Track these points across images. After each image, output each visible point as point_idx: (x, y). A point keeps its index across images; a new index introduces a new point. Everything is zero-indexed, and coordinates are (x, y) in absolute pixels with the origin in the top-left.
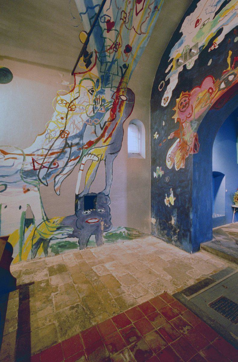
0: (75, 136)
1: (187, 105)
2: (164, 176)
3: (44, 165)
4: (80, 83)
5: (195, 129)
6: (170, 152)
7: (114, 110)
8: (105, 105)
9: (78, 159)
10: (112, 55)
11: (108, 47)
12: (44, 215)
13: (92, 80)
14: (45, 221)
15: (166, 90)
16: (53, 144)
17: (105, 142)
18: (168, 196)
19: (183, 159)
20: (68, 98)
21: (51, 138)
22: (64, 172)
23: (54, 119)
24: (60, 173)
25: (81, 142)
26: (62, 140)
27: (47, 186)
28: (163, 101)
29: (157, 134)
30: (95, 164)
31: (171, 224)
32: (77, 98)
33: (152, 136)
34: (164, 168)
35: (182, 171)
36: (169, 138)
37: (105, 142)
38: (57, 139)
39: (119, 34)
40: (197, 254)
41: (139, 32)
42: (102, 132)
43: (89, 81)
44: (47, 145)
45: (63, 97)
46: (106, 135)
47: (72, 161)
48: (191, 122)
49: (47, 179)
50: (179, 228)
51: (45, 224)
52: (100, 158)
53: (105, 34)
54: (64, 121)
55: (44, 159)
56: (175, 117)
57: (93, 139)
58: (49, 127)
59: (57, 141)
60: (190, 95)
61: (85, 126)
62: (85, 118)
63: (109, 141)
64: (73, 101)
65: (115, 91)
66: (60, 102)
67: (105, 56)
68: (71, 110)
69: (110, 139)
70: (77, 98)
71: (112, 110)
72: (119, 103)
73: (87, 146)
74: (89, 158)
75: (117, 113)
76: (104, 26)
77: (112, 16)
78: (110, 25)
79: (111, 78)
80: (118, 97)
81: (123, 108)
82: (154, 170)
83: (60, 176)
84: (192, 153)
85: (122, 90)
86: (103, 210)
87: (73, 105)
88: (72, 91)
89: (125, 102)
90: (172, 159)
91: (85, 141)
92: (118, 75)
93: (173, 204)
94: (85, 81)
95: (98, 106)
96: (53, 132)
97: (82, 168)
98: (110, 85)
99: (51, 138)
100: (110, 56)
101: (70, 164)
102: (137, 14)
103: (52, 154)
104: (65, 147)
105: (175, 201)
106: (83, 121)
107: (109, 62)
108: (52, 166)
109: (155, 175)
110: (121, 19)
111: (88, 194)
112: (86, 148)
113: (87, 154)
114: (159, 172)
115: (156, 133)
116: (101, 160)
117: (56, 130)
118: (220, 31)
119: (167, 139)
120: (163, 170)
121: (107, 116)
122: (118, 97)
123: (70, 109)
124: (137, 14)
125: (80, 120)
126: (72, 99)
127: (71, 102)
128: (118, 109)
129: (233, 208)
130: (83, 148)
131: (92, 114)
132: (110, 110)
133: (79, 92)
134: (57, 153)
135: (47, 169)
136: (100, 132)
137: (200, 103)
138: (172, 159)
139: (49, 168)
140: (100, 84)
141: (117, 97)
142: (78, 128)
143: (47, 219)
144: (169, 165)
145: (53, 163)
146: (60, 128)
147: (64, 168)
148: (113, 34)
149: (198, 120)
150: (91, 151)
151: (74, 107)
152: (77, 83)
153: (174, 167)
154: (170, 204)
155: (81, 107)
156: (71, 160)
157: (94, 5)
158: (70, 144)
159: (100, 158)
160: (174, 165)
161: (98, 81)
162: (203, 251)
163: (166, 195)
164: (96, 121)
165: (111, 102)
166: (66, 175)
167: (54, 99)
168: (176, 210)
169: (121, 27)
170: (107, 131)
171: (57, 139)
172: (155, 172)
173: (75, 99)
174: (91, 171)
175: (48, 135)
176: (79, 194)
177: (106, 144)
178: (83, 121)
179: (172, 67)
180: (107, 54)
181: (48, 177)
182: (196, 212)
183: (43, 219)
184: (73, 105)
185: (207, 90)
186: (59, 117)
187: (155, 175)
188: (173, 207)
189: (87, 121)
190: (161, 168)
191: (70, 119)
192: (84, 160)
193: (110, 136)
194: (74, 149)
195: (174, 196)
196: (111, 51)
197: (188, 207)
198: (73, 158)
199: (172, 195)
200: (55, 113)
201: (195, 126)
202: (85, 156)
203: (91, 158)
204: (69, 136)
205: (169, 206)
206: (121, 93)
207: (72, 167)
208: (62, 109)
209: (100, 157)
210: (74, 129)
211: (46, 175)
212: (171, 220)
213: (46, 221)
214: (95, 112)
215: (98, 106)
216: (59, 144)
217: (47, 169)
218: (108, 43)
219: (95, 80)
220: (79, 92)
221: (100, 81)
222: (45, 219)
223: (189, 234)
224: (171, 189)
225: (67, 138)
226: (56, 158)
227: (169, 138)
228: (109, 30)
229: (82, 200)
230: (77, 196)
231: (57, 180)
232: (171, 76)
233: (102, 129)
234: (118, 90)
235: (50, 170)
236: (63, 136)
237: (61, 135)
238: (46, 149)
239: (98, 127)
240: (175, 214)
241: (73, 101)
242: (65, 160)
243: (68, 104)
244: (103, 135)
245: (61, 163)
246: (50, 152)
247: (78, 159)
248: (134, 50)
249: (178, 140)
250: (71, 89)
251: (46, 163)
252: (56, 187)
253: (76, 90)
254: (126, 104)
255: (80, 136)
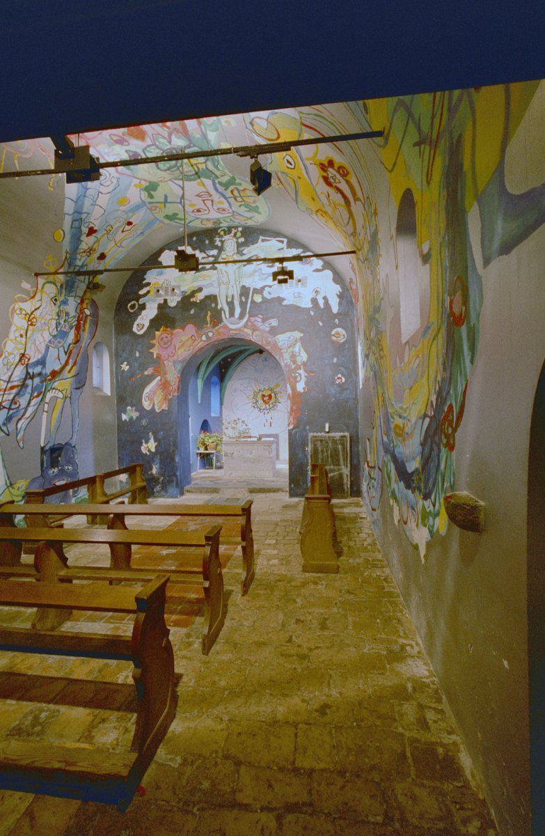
0: (38, 363)
1: (169, 343)
2: (139, 419)
3: (3, 404)
4: (42, 288)
5: (179, 370)
6: (147, 390)
7: (78, 328)
8: (69, 320)
9: (41, 396)
10: (83, 259)
11: (82, 251)
12: (7, 479)
13: (56, 285)
14: (8, 487)
15: (140, 315)
16: (12, 374)
17: (69, 372)
18: (147, 442)
19: (165, 399)
20: (28, 306)
21: (10, 364)
22: (28, 414)
23: (11, 336)
24: (22, 416)
25: (44, 372)
26: (22, 367)
27: (8, 435)
28: (135, 326)
29: (127, 365)
30: (60, 402)
31: (152, 474)
32: (39, 308)
33: (118, 367)
34: (140, 408)
35: (165, 412)
36: (146, 373)
37: (69, 372)
38: (16, 366)
39: (98, 241)
40: (184, 497)
41: (118, 244)
42: (66, 358)
43: (53, 285)
44: (5, 374)
45: (21, 305)
46: (71, 361)
47: (35, 399)
48: (174, 362)
49: (8, 425)
50: (163, 475)
51: (8, 493)
52: (64, 393)
53: (83, 237)
54: (24, 339)
55: (3, 395)
56: (155, 351)
57: (57, 368)
58: (6, 349)
59: (16, 369)
60: (172, 334)
61: (47, 348)
62: (47, 337)
63: (73, 373)
64: (33, 312)
65: (79, 302)
66: (18, 312)
67: (76, 259)
68: (31, 325)
69: (75, 367)
70: (39, 308)
71: (76, 328)
72: (84, 319)
73: (50, 377)
74: (53, 395)
75: (81, 332)
76: (85, 230)
77: (97, 225)
78: (92, 231)
79: (76, 284)
80: (82, 311)
81: (87, 326)
82: (121, 410)
83: (23, 420)
84: (176, 394)
85: (86, 301)
86: (70, 468)
87: (33, 318)
88: (33, 297)
89: (89, 318)
90: (151, 399)
91: (48, 370)
92: (84, 282)
93: (153, 450)
94: (48, 285)
95: (62, 322)
96: (12, 356)
97: (46, 409)
98: (74, 294)
99: (10, 364)
100: (80, 260)
101: (33, 402)
102: (123, 232)
103: (12, 388)
104: (25, 379)
105: (156, 447)
106: (45, 341)
107: (78, 266)
108: (13, 406)
109: (124, 417)
110: (105, 230)
111: (54, 445)
112: (50, 380)
113: (51, 388)
114: (130, 414)
115: (126, 363)
116: (66, 398)
117: (15, 353)
118: (200, 290)
119: (143, 374)
120: (138, 411)
121: (71, 337)
122: (82, 311)
123: (30, 323)
124: (123, 232)
125: (41, 340)
126: (33, 309)
127: (32, 313)
128: (82, 328)
129: (197, 454)
130: (46, 380)
131: (55, 333)
132: (74, 327)
133: (41, 300)
134: (17, 386)
135: (7, 410)
136: (64, 358)
137: (183, 344)
138: (151, 399)
139: (9, 409)
140: (64, 291)
141: (81, 310)
142: (40, 352)
143: (11, 485)
144: (146, 405)
145: (13, 401)
146: (19, 349)
147: (26, 409)
148: (92, 239)
149: (181, 362)
150: (56, 385)
151: (35, 320)
152: (40, 286)
153: (153, 408)
154: (149, 451)
155: (43, 322)
156: (34, 398)
157: (84, 211)
158: (31, 374)
159: (64, 393)
160: (154, 405)
161: (62, 286)
162: (188, 494)
163: (143, 441)
164: (59, 342)
165: (74, 317)
166: (29, 420)
167: (12, 306)
168: (159, 456)
169: (103, 236)
170: (71, 357)
171: (16, 366)
172: (125, 414)
173: (36, 309)
174: (56, 414)
175: (6, 360)
176: (44, 447)
177: (70, 375)
178: (45, 341)
179: (149, 292)
180: (79, 257)
181: (9, 422)
182: (180, 455)
183: (6, 484)
184: (33, 318)
185: (190, 336)
186: (18, 334)
187: (124, 417)
188: (153, 455)
189: (50, 342)
190: (134, 408)
191: (30, 337)
192: (49, 396)
193: (75, 363)
194: (37, 380)
195: (155, 441)
196: (84, 254)
197: (173, 451)
198: (36, 394)
199: (152, 440)
200: (13, 328)
201: (179, 367)
202: (49, 391)
203: (56, 395)
204: (30, 362)
205: (148, 453)
206: (85, 306)
207: (35, 407)
208: (19, 322)
209: (64, 392)
210: (35, 353)
211: (6, 419)
212: (151, 469)
213: (10, 489)
214: (59, 329)
215: (62, 322)
216: (19, 373)
217: (7, 410)
218: (84, 246)
219: (59, 285)
220: (41, 300)
221: (64, 287)
222: (9, 484)
223: (175, 479)
224: (150, 433)
225: (27, 365)
226: (17, 394)
227: (146, 373)
228: (88, 235)
229: (48, 453)
230: (42, 449)
231: (19, 426)
232: (148, 301)
233: (66, 353)
234: (82, 302)
235: (11, 412)
236: (23, 362)
237: (20, 360)
238: (5, 381)
239: (61, 349)
240: (157, 461)
241: (33, 312)
242: (27, 397)
243: (28, 316)
244: (67, 363)
245: (23, 401)
246: (10, 385)
247: (41, 396)
248: (107, 260)
249: (159, 378)
250: (32, 295)
251: (6, 401)
252: (19, 437)
253: (38, 297)
254: (91, 320)
255: (42, 362)
